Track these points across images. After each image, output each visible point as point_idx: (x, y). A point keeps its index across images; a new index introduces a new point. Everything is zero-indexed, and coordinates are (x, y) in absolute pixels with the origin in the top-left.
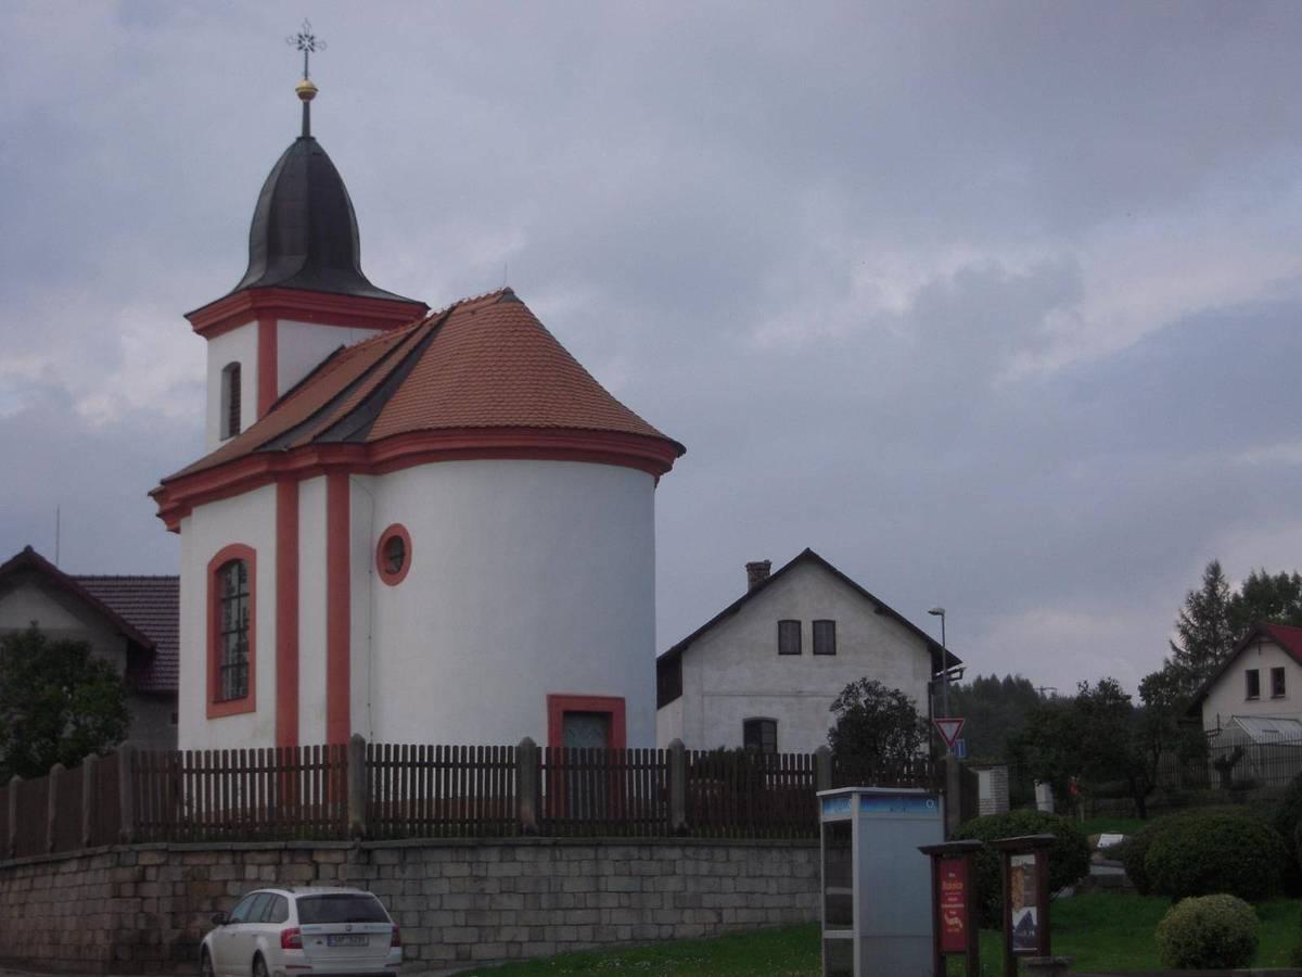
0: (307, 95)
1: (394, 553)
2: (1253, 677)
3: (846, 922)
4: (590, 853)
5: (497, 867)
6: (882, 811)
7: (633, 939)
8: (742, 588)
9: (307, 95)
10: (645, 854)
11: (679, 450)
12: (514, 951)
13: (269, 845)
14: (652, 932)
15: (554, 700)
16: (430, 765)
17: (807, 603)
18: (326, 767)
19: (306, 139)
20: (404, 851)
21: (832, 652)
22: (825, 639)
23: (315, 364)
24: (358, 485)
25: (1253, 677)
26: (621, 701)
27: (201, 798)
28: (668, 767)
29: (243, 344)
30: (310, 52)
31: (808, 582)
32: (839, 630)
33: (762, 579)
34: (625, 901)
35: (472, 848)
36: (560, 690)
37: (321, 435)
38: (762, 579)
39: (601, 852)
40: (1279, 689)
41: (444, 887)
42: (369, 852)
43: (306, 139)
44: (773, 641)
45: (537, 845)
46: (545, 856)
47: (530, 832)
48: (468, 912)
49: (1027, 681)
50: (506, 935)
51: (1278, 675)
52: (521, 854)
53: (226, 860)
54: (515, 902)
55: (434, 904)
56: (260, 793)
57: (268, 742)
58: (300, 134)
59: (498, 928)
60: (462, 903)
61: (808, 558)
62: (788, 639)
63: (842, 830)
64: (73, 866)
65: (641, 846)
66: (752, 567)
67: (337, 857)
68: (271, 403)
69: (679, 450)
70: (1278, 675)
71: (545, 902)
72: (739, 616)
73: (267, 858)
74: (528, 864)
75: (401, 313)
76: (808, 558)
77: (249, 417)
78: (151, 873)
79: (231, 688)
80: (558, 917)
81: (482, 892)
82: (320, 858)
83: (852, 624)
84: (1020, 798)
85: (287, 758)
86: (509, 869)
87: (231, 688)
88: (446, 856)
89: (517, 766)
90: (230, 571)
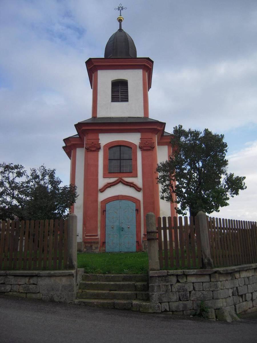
0: (120, 21)
19: (120, 30)
30: (122, 11)
58: (119, 28)
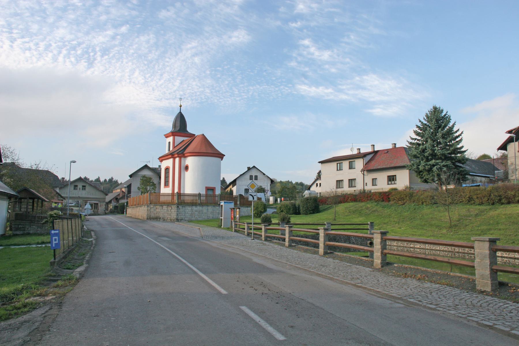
1: (187, 168)
2: (317, 184)
3: (222, 217)
4: (207, 207)
5: (194, 208)
6: (226, 204)
7: (212, 218)
8: (247, 170)
9: (181, 106)
10: (214, 207)
11: (225, 155)
12: (197, 219)
13: (28, 222)
14: (215, 217)
15: (206, 187)
16: (188, 196)
17: (254, 173)
18: (171, 195)
19: (180, 112)
20: (183, 206)
21: (257, 180)
22: (256, 178)
23: (181, 141)
24: (182, 159)
25: (317, 184)
26: (215, 188)
27: (162, 199)
28: (218, 197)
29: (171, 139)
31: (254, 170)
32: (258, 177)
33: (249, 169)
34: (211, 213)
35: (191, 206)
36: (207, 186)
37: (178, 152)
38: (249, 169)
39: (208, 207)
40: (320, 186)
41: (188, 211)
42: (178, 206)
43: (180, 112)
44: (249, 178)
45: (200, 206)
46: (201, 207)
47: (199, 204)
48: (191, 214)
49: (301, 182)
50: (196, 217)
51: (320, 184)
52: (198, 207)
53: (161, 207)
54: (197, 213)
55: (186, 213)
56: (169, 199)
57: (171, 192)
59: (195, 216)
60: (190, 213)
61: (254, 167)
62: (251, 178)
63: (222, 206)
64: (143, 207)
65: (214, 206)
66: (248, 168)
67: (174, 207)
68: (174, 147)
69: (225, 155)
70: (320, 184)
71: (201, 213)
72: (244, 174)
73: (166, 206)
74: (199, 208)
75: (192, 136)
76: (254, 167)
77: (171, 149)
78: (152, 208)
79: (166, 184)
80: (203, 215)
81: (193, 212)
82: (172, 207)
83: (260, 176)
84: (276, 200)
85: (173, 194)
86: (196, 209)
87: (166, 184)
88: (188, 207)
89: (198, 196)
90: (167, 169)
